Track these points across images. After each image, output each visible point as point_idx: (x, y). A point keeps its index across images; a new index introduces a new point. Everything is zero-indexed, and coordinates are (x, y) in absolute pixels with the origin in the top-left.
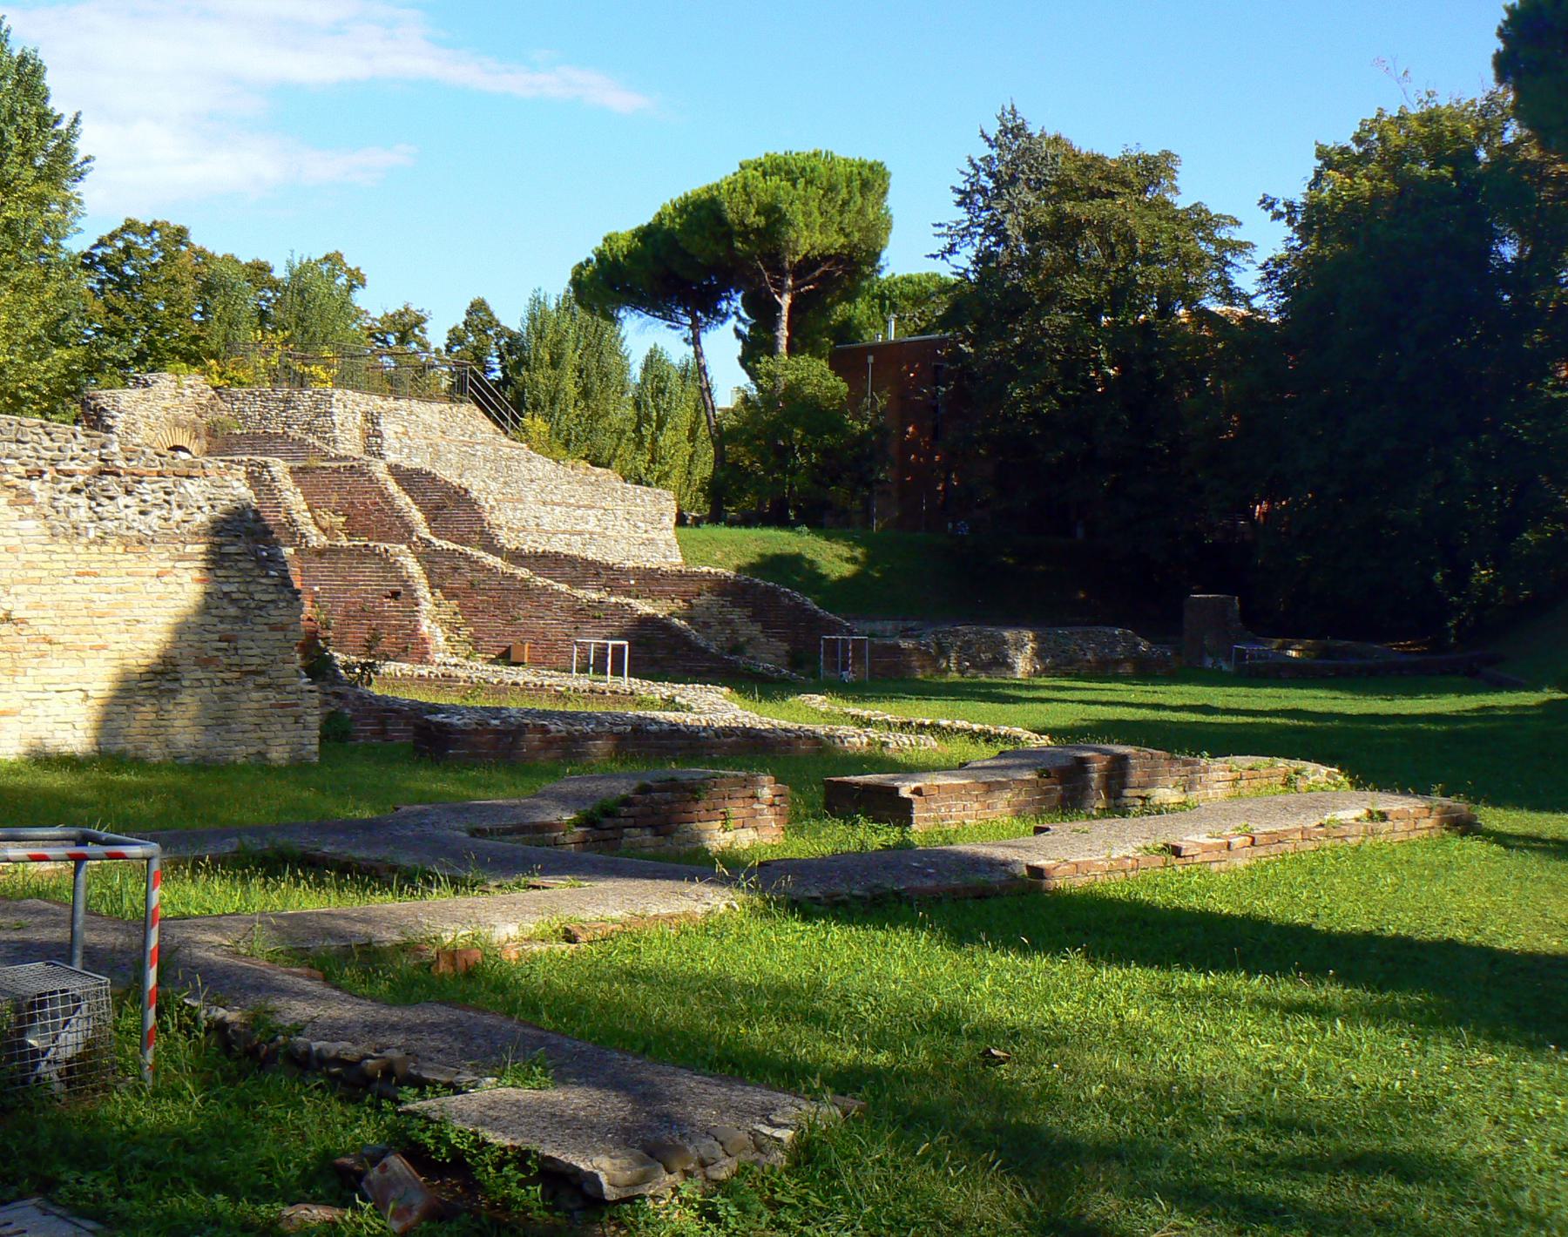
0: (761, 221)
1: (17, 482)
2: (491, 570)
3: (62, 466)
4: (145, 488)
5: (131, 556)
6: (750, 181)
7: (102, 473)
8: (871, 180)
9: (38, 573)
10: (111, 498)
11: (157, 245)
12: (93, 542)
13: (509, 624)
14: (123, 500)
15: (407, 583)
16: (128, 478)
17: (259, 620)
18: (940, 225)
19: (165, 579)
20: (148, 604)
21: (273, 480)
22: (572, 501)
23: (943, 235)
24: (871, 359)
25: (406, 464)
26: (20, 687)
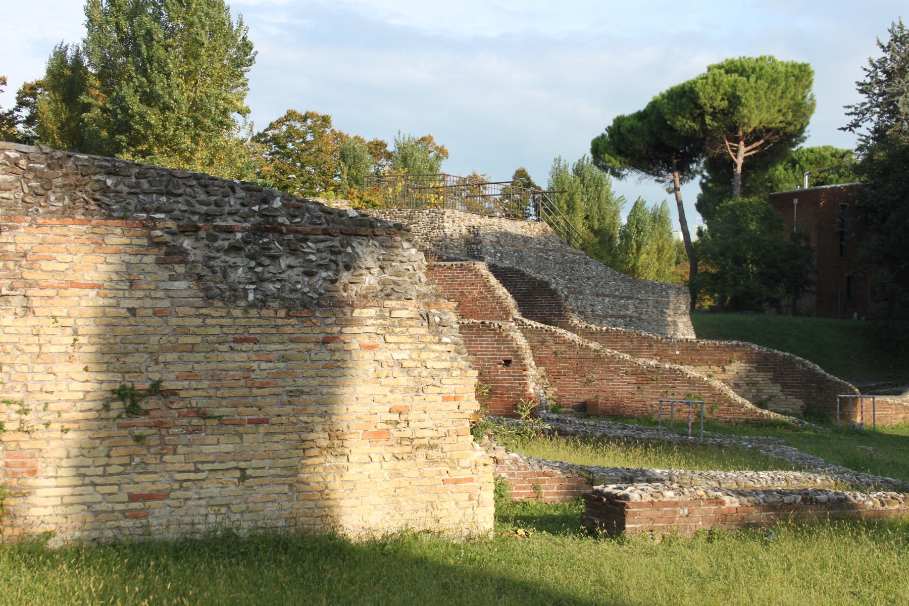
0: (725, 104)
1: (168, 238)
2: (571, 344)
3: (219, 222)
5: (293, 321)
6: (717, 77)
8: (801, 75)
9: (190, 340)
11: (310, 128)
12: (252, 305)
13: (586, 384)
15: (516, 352)
16: (291, 236)
18: (849, 107)
20: (313, 373)
22: (617, 293)
23: (852, 114)
24: (796, 201)
25: (499, 264)
26: (169, 467)
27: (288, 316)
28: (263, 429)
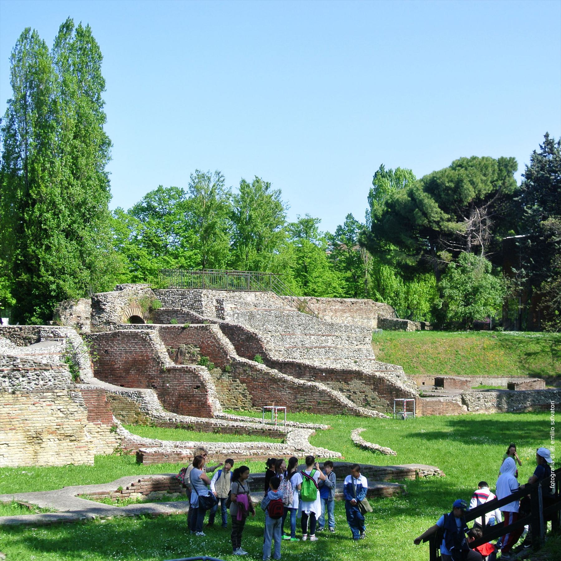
4: (30, 374)
7: (14, 370)
10: (17, 378)
14: (21, 379)
16: (23, 371)
17: (71, 418)
19: (36, 405)
21: (150, 339)
27: (22, 396)
28: (14, 431)
